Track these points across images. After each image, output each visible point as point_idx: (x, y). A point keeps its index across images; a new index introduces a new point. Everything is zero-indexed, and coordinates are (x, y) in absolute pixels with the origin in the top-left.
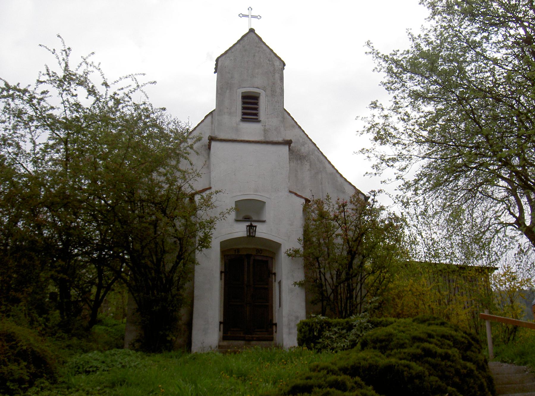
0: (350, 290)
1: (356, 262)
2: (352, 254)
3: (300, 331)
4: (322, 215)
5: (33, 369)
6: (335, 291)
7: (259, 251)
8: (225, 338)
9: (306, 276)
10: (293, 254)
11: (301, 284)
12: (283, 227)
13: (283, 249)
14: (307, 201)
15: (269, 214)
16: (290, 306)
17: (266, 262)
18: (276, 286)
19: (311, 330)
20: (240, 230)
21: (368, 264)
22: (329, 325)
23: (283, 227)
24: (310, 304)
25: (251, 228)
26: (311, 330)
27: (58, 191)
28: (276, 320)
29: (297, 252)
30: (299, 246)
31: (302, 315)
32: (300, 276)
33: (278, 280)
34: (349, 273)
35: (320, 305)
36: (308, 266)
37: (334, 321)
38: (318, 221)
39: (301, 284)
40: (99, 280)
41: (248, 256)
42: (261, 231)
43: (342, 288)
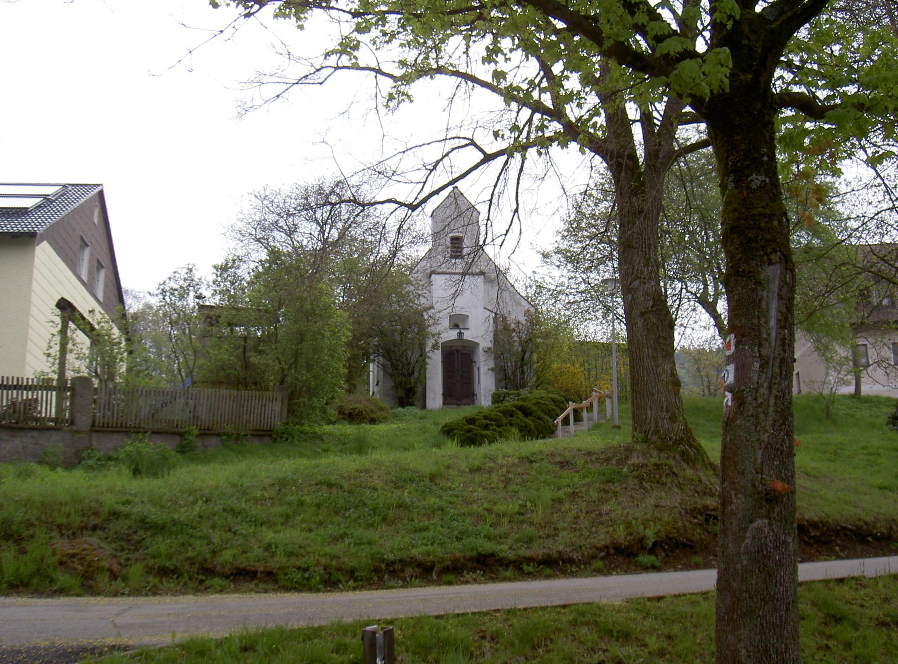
0: (523, 372)
1: (527, 355)
2: (524, 351)
3: (493, 397)
4: (506, 328)
5: (775, 257)
6: (514, 373)
7: (465, 347)
8: (444, 403)
9: (495, 364)
10: (488, 351)
11: (492, 369)
12: (479, 332)
13: (481, 347)
14: (496, 314)
15: (471, 323)
16: (486, 384)
17: (469, 354)
18: (476, 369)
19: (499, 397)
20: (453, 335)
21: (535, 357)
22: (509, 394)
23: (479, 332)
24: (498, 381)
25: (460, 334)
26: (499, 397)
27: (424, 330)
28: (476, 392)
29: (490, 349)
30: (491, 345)
31: (493, 388)
32: (492, 364)
33: (477, 366)
34: (523, 362)
35: (504, 382)
36: (497, 357)
37: (513, 391)
38: (502, 328)
39: (492, 369)
40: (741, 326)
41: (458, 351)
42: (468, 335)
43: (518, 373)
